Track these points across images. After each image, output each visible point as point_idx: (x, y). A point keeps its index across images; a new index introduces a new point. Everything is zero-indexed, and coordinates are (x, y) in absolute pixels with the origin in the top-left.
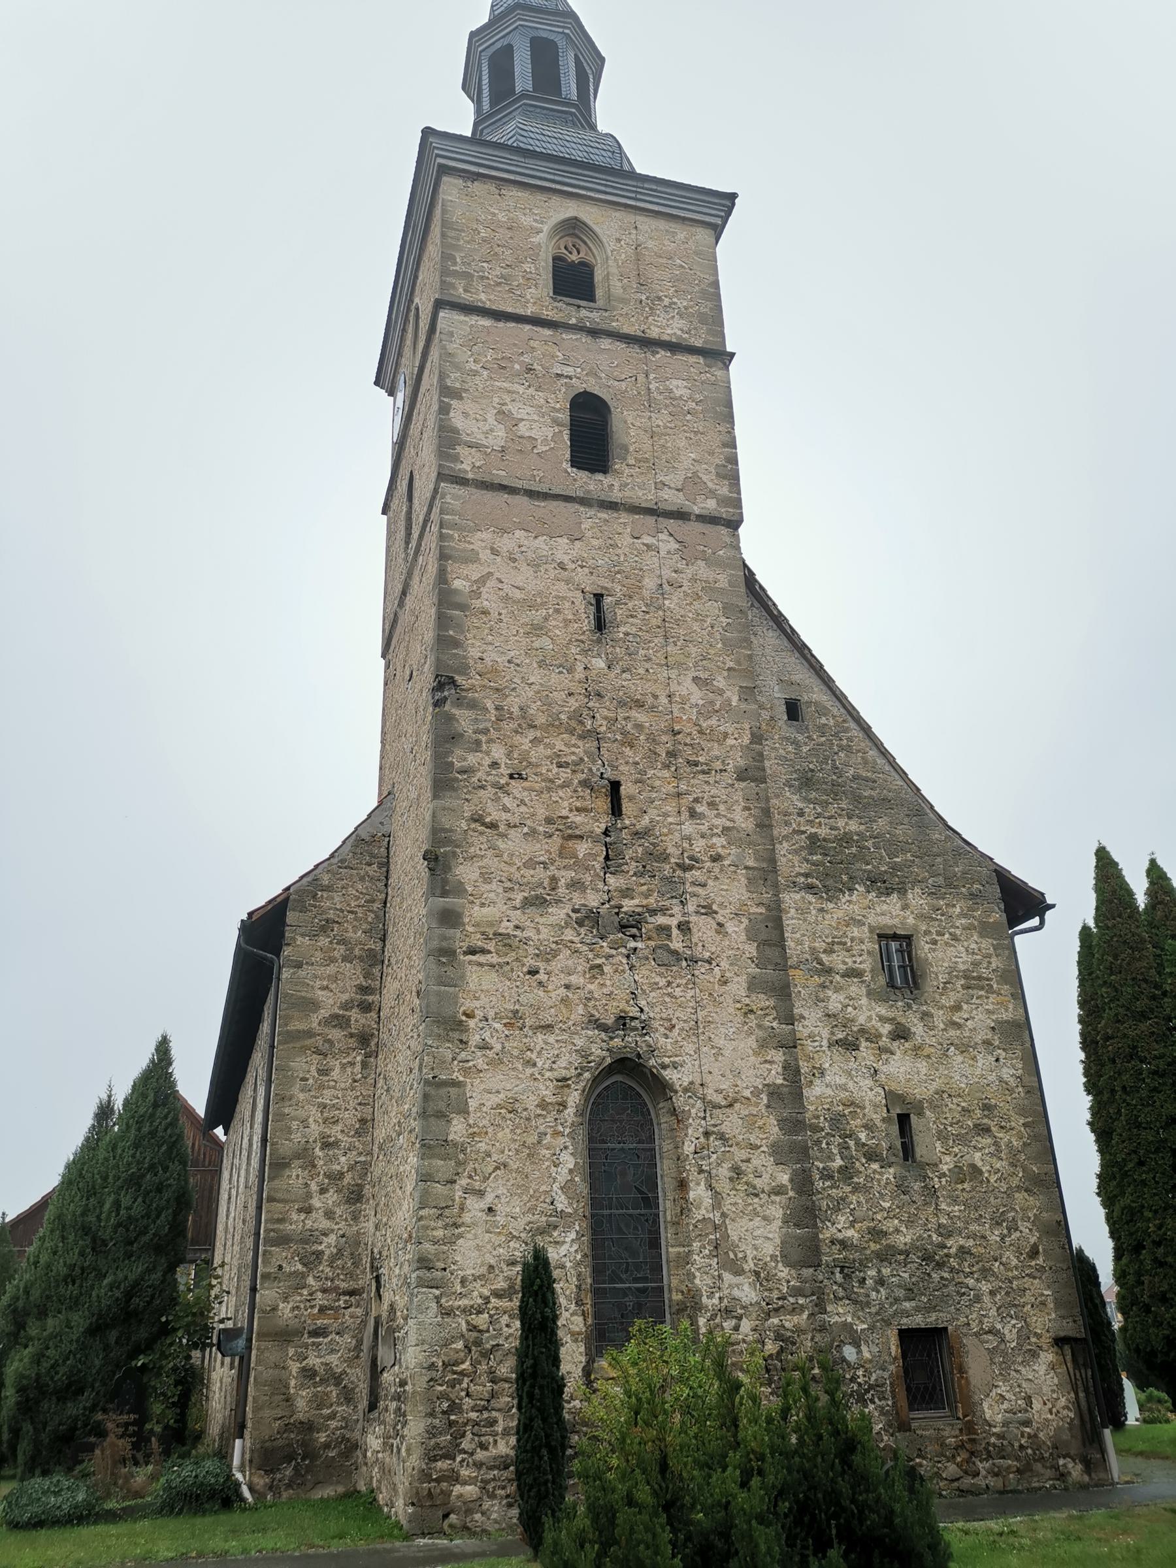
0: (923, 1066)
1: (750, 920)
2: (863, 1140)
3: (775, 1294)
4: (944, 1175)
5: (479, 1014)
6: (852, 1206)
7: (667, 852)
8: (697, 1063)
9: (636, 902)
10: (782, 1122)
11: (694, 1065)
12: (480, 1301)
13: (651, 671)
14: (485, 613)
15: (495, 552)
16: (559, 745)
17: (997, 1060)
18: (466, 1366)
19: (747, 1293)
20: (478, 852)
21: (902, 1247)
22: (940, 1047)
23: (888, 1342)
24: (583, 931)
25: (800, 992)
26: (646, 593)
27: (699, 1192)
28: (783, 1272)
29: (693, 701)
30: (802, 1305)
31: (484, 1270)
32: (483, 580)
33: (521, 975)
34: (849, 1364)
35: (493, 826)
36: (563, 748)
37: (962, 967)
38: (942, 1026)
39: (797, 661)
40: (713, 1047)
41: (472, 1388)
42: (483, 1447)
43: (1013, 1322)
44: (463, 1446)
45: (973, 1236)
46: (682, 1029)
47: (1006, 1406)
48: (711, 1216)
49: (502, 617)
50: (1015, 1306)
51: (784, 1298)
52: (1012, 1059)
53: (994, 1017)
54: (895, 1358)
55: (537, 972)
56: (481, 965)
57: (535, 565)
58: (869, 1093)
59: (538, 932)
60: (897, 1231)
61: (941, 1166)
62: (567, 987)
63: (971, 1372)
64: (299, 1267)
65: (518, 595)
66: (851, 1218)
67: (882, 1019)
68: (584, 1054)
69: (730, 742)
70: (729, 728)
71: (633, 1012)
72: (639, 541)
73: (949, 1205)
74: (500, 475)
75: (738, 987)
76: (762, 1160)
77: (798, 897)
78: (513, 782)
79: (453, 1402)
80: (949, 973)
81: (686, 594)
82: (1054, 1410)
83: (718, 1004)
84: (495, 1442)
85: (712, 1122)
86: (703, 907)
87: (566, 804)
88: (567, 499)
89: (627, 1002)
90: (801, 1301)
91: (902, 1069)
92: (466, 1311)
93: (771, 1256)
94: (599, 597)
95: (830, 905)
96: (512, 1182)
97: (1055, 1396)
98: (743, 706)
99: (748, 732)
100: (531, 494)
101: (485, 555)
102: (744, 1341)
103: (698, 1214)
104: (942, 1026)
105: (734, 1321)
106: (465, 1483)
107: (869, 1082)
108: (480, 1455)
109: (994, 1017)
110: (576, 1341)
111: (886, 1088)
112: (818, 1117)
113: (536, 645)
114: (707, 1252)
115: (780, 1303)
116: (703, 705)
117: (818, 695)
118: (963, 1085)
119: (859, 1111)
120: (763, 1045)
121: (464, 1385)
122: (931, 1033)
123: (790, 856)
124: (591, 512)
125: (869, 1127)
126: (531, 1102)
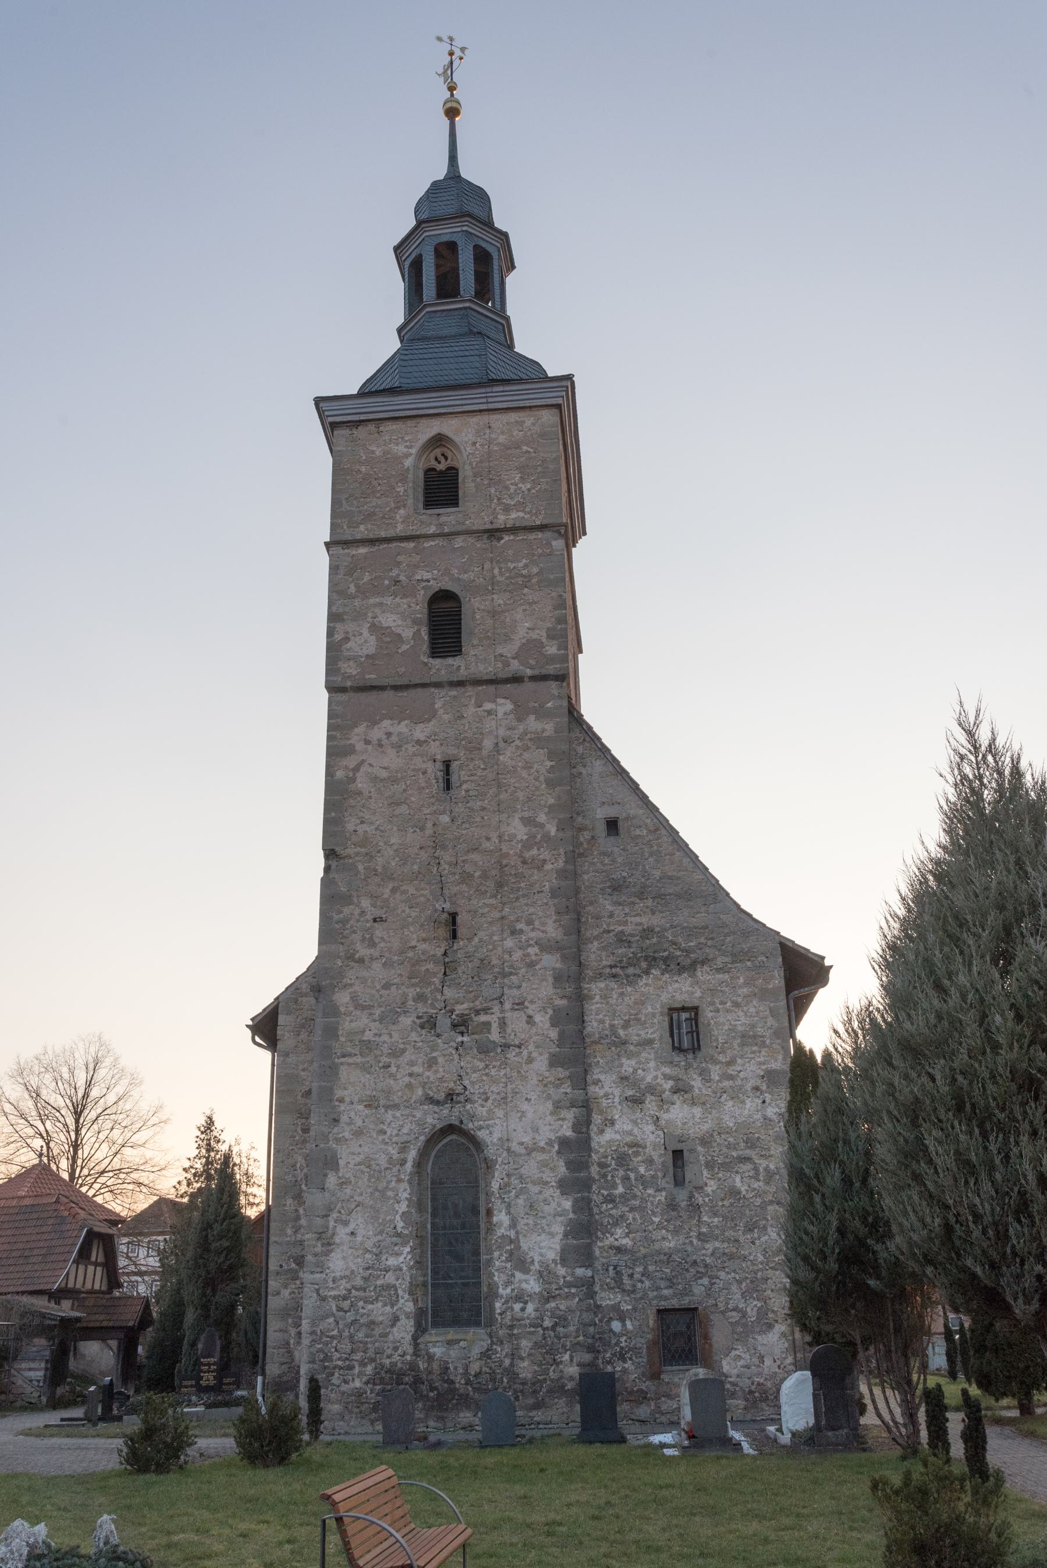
0: (697, 1111)
1: (554, 1011)
2: (643, 1172)
3: (554, 1286)
4: (708, 1195)
5: (347, 1099)
6: (628, 1222)
7: (492, 964)
8: (505, 1124)
9: (465, 1006)
10: (569, 1164)
11: (502, 1126)
12: (344, 1292)
13: (486, 818)
14: (360, 793)
15: (367, 742)
16: (412, 890)
17: (764, 1102)
18: (335, 1332)
19: (532, 1285)
20: (349, 982)
21: (667, 1250)
22: (713, 1095)
23: (648, 1317)
24: (424, 1032)
25: (598, 1062)
26: (485, 752)
27: (500, 1217)
28: (561, 1271)
29: (519, 837)
30: (573, 1294)
31: (348, 1273)
32: (357, 769)
33: (378, 1069)
34: (614, 1333)
35: (361, 961)
36: (414, 892)
37: (740, 1028)
38: (717, 1078)
39: (620, 783)
40: (518, 1111)
41: (339, 1346)
42: (346, 1382)
43: (755, 1303)
44: (333, 1381)
45: (729, 1241)
46: (494, 1100)
47: (742, 1363)
48: (508, 1233)
49: (372, 794)
50: (758, 1291)
51: (560, 1289)
52: (777, 1100)
53: (764, 1067)
54: (653, 1329)
55: (390, 1066)
56: (349, 1064)
57: (398, 747)
58: (649, 1135)
59: (391, 1036)
60: (664, 1239)
61: (706, 1188)
62: (411, 1075)
63: (714, 1339)
64: (293, 1265)
65: (384, 774)
66: (627, 1231)
67: (667, 1077)
68: (421, 1123)
69: (548, 867)
70: (545, 854)
71: (459, 1089)
72: (481, 709)
73: (710, 1217)
74: (372, 677)
75: (541, 1063)
76: (552, 1192)
77: (602, 985)
78: (376, 925)
79: (327, 1355)
80: (728, 1035)
81: (517, 747)
82: (782, 1366)
83: (524, 1078)
84: (353, 1379)
85: (515, 1167)
86: (517, 1004)
87: (415, 936)
88: (424, 685)
89: (455, 1082)
90: (573, 1290)
91: (681, 1115)
92: (334, 1298)
93: (553, 1260)
94: (447, 765)
95: (629, 989)
96: (367, 1214)
97: (784, 1356)
98: (561, 835)
99: (563, 856)
100: (396, 688)
101: (360, 746)
102: (528, 1318)
103: (501, 1232)
104: (717, 1078)
105: (521, 1305)
106: (333, 1403)
107: (651, 1128)
108: (344, 1388)
109: (764, 1067)
110: (408, 1318)
111: (665, 1131)
112: (606, 1157)
113: (397, 812)
114: (504, 1258)
115: (557, 1292)
116: (527, 839)
117: (634, 809)
118: (731, 1125)
119: (641, 1150)
120: (557, 1106)
121: (334, 1345)
122: (708, 1085)
123: (599, 952)
124: (443, 692)
125: (650, 1161)
126: (383, 1161)
